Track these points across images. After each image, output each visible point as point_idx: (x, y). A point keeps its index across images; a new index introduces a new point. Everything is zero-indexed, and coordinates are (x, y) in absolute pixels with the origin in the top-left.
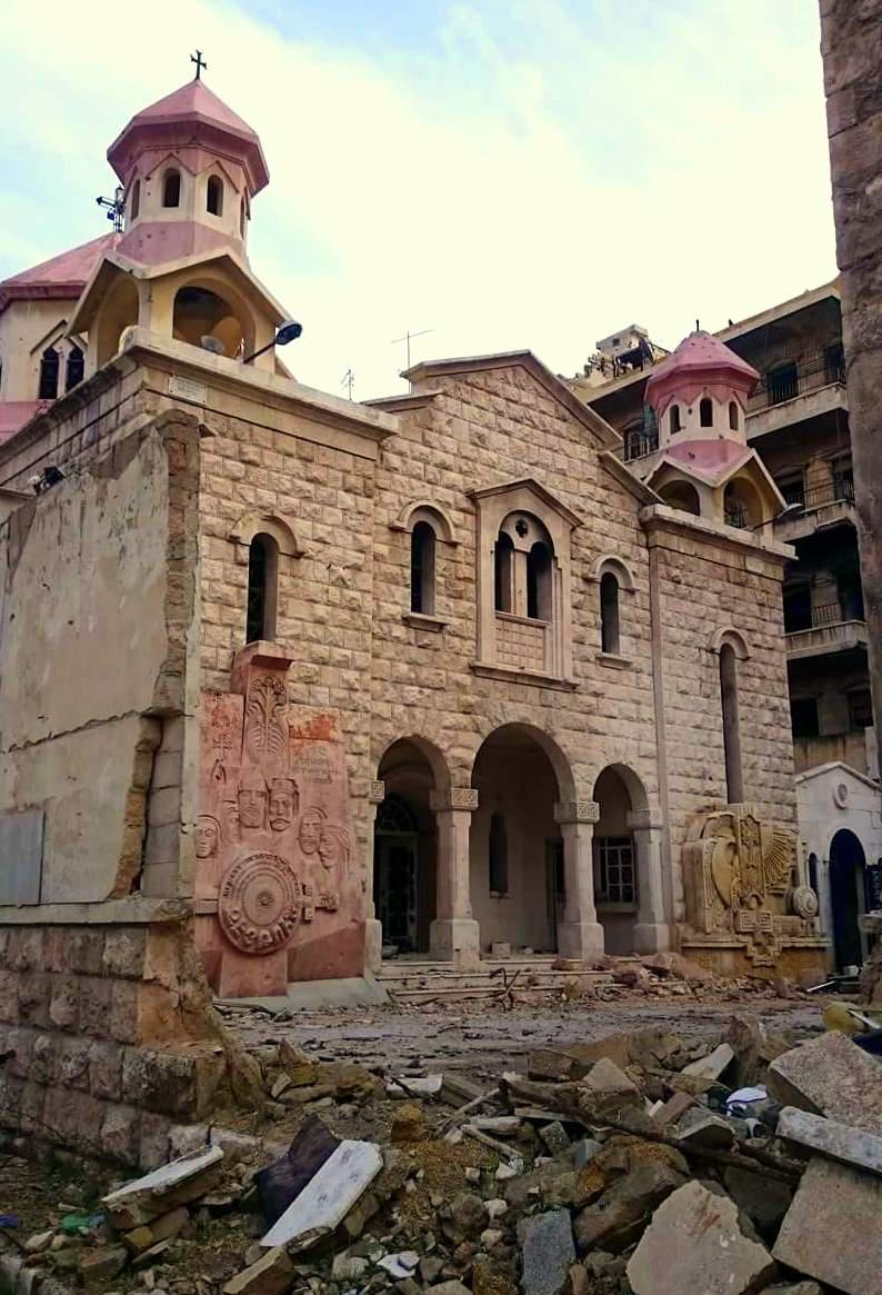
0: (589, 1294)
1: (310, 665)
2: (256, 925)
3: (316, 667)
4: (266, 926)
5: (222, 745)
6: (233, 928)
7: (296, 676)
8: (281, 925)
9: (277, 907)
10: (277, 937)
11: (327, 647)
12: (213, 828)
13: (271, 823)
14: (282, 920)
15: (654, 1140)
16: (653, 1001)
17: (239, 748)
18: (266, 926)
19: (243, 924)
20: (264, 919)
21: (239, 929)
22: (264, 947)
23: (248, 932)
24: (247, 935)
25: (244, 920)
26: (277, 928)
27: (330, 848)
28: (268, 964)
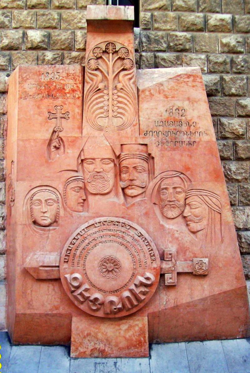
0: (244, 43)
1: (179, 34)
2: (100, 290)
3: (188, 35)
4: (114, 292)
5: (59, 115)
6: (75, 294)
7: (165, 45)
8: (131, 291)
9: (125, 275)
10: (127, 303)
11: (201, 15)
12: (54, 197)
13: (123, 189)
14: (133, 287)
15: (124, 110)
16: (197, 261)
17: (79, 117)
18: (114, 292)
19: (86, 290)
20: (113, 284)
21: (81, 294)
22: (112, 312)
23: (92, 298)
24: (91, 301)
25: (86, 286)
26: (127, 294)
27: (197, 211)
28: (124, 327)
